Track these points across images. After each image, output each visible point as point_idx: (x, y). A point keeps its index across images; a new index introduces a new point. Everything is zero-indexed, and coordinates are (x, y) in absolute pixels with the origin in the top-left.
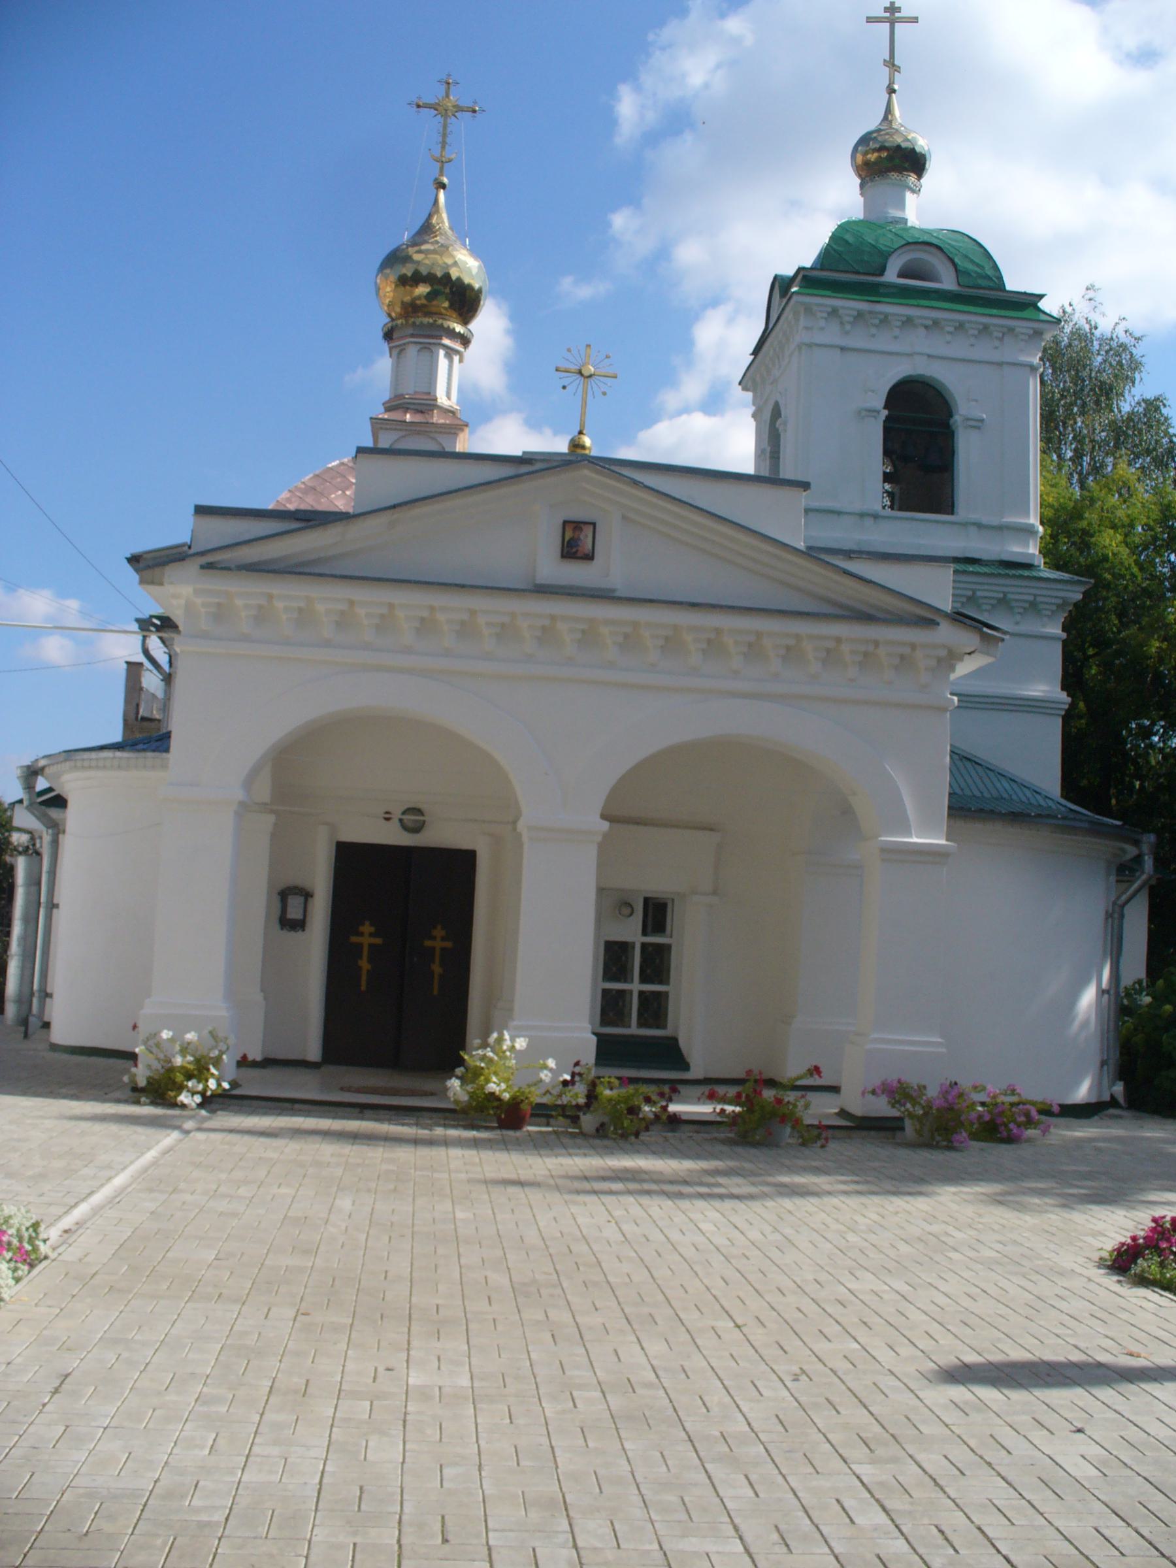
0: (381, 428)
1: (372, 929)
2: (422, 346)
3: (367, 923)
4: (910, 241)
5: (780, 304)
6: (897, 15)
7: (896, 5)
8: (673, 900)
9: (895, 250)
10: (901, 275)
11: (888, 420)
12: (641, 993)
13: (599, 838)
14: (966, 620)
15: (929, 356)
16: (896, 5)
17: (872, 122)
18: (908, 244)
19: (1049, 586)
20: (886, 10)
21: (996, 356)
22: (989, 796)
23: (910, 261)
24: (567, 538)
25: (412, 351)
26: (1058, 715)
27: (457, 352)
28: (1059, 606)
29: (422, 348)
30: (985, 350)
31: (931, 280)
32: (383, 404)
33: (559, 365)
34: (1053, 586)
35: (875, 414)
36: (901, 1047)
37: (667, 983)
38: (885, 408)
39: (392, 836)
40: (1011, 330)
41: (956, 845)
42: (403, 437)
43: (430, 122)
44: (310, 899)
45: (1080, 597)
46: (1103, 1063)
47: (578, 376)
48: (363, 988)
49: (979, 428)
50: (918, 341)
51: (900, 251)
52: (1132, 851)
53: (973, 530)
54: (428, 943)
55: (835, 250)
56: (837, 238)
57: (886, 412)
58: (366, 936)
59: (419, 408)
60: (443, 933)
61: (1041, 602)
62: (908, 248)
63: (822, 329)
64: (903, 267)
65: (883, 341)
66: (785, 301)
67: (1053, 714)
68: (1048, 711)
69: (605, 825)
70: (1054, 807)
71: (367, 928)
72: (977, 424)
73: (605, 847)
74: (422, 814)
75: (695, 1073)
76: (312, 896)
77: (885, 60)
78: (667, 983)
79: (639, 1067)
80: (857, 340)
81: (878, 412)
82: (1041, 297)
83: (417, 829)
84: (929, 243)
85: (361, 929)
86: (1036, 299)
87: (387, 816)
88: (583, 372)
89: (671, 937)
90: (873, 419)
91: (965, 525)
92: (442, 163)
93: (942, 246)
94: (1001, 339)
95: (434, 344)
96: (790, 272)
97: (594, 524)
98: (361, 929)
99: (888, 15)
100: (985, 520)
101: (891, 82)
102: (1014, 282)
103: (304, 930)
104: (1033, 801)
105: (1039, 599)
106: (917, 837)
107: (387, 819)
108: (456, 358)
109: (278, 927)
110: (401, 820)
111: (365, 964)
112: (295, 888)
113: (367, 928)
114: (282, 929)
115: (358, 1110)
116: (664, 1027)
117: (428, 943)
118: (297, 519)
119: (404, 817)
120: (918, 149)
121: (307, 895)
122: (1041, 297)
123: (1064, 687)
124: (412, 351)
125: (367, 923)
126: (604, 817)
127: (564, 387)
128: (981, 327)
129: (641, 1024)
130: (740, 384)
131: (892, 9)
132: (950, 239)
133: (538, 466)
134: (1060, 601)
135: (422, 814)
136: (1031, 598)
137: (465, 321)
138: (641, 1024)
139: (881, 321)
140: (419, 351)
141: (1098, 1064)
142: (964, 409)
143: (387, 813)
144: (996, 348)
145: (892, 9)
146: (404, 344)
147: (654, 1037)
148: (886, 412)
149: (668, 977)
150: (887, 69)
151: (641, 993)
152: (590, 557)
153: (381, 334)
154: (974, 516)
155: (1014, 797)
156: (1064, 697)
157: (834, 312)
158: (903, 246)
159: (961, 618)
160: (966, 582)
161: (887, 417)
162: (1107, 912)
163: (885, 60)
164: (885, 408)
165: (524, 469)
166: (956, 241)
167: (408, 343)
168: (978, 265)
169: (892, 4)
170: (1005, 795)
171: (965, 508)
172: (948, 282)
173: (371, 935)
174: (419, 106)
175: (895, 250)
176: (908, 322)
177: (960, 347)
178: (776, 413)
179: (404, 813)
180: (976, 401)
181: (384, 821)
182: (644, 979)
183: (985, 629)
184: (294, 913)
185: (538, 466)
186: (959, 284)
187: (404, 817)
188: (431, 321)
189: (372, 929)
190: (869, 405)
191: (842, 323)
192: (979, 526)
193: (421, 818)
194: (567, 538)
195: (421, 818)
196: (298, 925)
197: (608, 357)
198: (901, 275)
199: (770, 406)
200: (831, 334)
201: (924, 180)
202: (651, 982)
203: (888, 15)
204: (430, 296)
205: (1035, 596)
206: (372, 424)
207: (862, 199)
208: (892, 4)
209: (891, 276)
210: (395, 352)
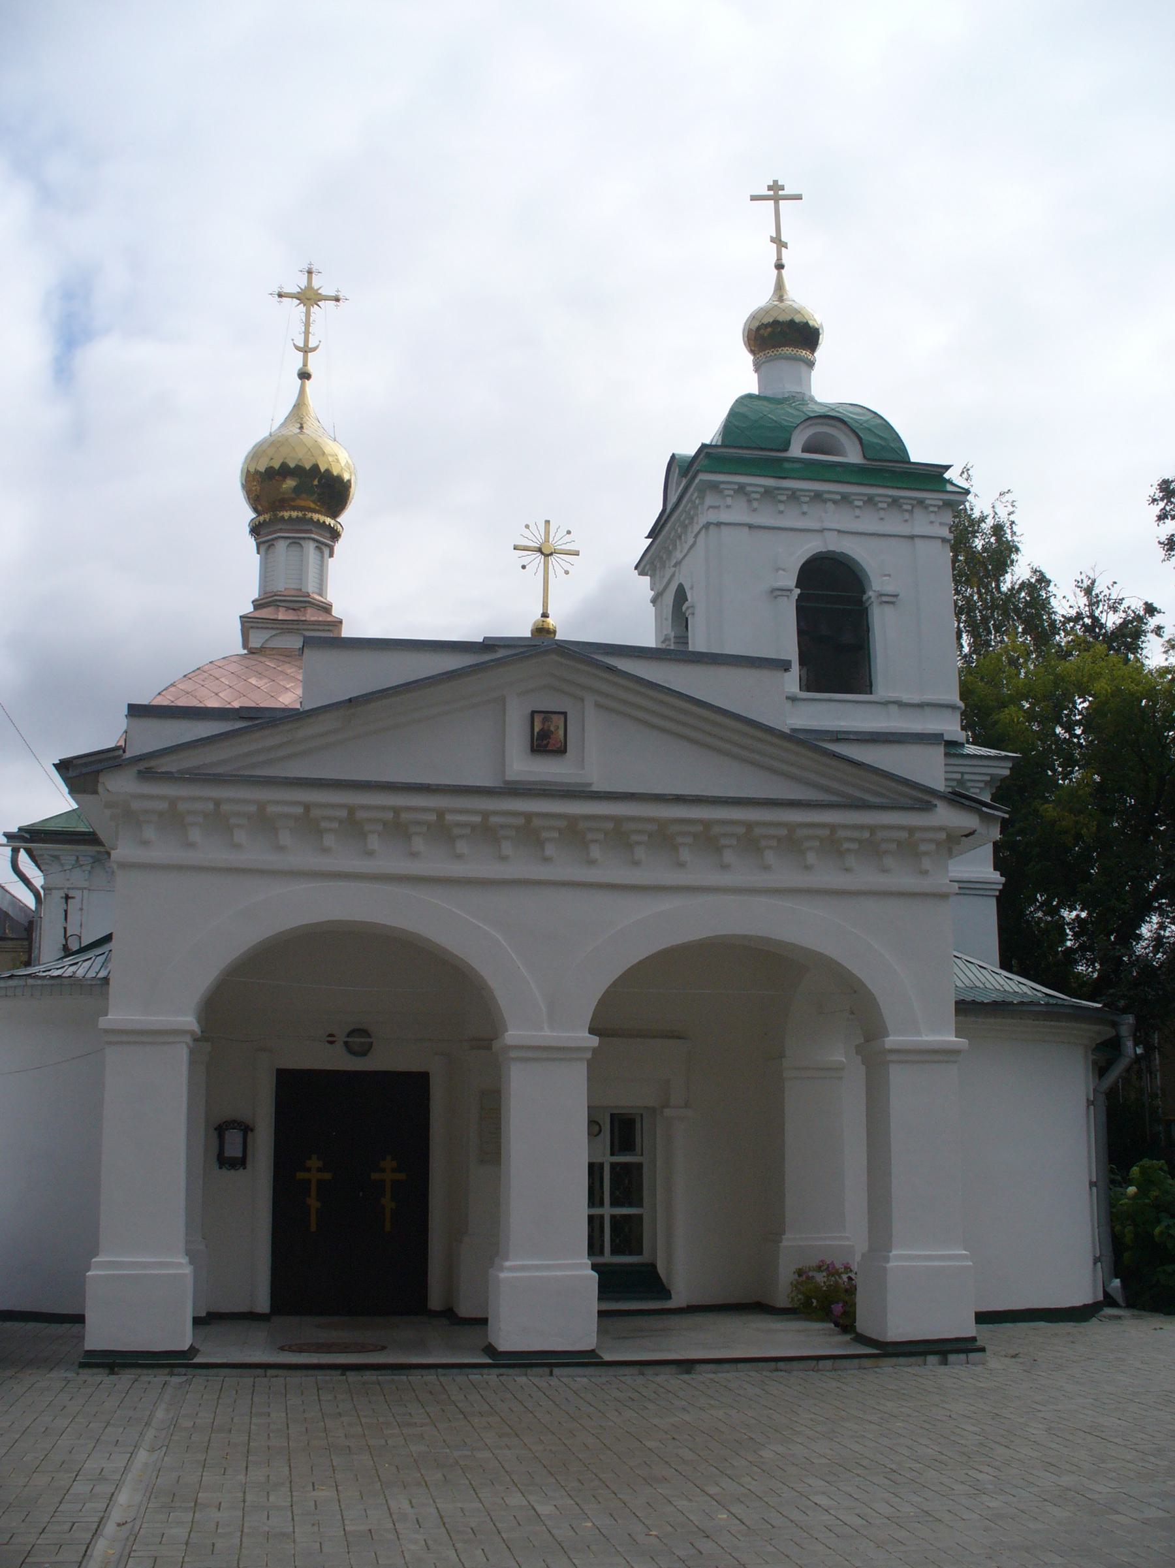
0: (252, 627)
1: (394, 1164)
2: (267, 545)
3: (314, 1157)
4: (812, 415)
5: (678, 485)
6: (781, 193)
7: (780, 183)
8: (642, 1115)
9: (798, 425)
10: (805, 449)
11: (800, 599)
12: (613, 1217)
13: (589, 1055)
14: (963, 801)
15: (839, 531)
16: (780, 183)
17: (759, 298)
18: (810, 418)
19: (981, 764)
20: (770, 188)
21: (905, 530)
22: (962, 985)
23: (810, 437)
24: (536, 730)
25: (281, 546)
26: (994, 896)
27: (326, 545)
28: (986, 783)
29: (290, 543)
30: (893, 523)
31: (834, 455)
32: (253, 602)
33: (517, 544)
34: (986, 763)
35: (788, 593)
36: (936, 1263)
37: (640, 1204)
38: (797, 587)
39: (337, 1060)
40: (921, 502)
41: (967, 1041)
42: (274, 635)
43: (296, 310)
44: (250, 1134)
45: (1007, 772)
46: (1096, 1260)
47: (539, 554)
48: (313, 1228)
49: (893, 603)
50: (835, 518)
51: (801, 427)
52: (1109, 1032)
53: (894, 709)
54: (301, 1175)
55: (737, 427)
56: (733, 414)
57: (798, 591)
58: (314, 1171)
59: (296, 605)
60: (320, 1164)
61: (969, 780)
62: (809, 422)
63: (728, 507)
64: (803, 445)
65: (791, 519)
66: (684, 482)
67: (986, 895)
68: (982, 892)
69: (594, 1041)
70: (1029, 993)
71: (314, 1163)
72: (890, 600)
73: (596, 1065)
74: (370, 1036)
75: (678, 1300)
76: (252, 1130)
77: (771, 237)
78: (640, 1204)
79: (617, 1300)
80: (765, 517)
81: (791, 591)
82: (947, 467)
83: (364, 1051)
84: (833, 418)
85: (309, 1163)
86: (944, 470)
87: (330, 1039)
88: (543, 550)
89: (642, 1155)
90: (786, 598)
91: (886, 703)
92: (306, 350)
93: (845, 419)
94: (911, 512)
95: (304, 538)
96: (690, 450)
97: (565, 714)
98: (309, 1163)
99: (771, 193)
100: (906, 697)
101: (779, 258)
102: (919, 453)
103: (245, 1168)
104: (1007, 988)
105: (967, 777)
106: (927, 1036)
107: (331, 1043)
108: (326, 551)
109: (216, 1166)
110: (346, 1043)
111: (314, 1203)
112: (234, 1121)
113: (314, 1163)
114: (220, 1168)
115: (339, 1372)
116: (640, 1253)
117: (301, 1175)
118: (242, 718)
119: (350, 1040)
120: (811, 323)
121: (246, 1129)
122: (947, 467)
123: (996, 867)
124: (281, 546)
125: (314, 1157)
126: (592, 1031)
127: (524, 567)
128: (890, 500)
129: (614, 1252)
130: (636, 568)
131: (775, 187)
132: (851, 413)
133: (501, 653)
134: (988, 778)
135: (370, 1036)
136: (958, 776)
137: (335, 515)
138: (614, 1252)
139: (789, 497)
140: (288, 546)
141: (1091, 1263)
142: (877, 584)
143: (331, 1035)
144: (906, 521)
145: (775, 187)
146: (273, 540)
147: (631, 1265)
148: (798, 591)
149: (641, 1199)
150: (775, 245)
151: (613, 1217)
152: (562, 751)
153: (248, 529)
154: (893, 695)
155: (988, 985)
156: (996, 877)
157: (741, 489)
158: (805, 420)
159: (958, 799)
160: (286, 803)
161: (799, 596)
162: (1088, 1100)
163: (771, 237)
164: (797, 587)
165: (486, 657)
166: (854, 414)
167: (276, 538)
168: (881, 438)
169: (776, 182)
170: (978, 984)
171: (883, 689)
172: (853, 456)
173: (319, 1170)
174: (280, 295)
175: (798, 425)
176: (818, 497)
177: (868, 522)
178: (681, 596)
179: (348, 1036)
180: (889, 575)
181: (328, 1045)
182: (615, 1203)
183: (984, 809)
184: (233, 1150)
185: (501, 653)
186: (865, 457)
187: (350, 1040)
188: (300, 514)
189: (394, 1164)
190: (779, 584)
191: (749, 501)
192: (900, 704)
193: (369, 1040)
194: (536, 730)
195: (369, 1040)
196: (240, 1163)
197: (569, 532)
198: (805, 449)
199: (673, 587)
200: (737, 512)
201: (818, 354)
202: (622, 1205)
203: (771, 193)
204: (297, 490)
205: (962, 774)
206: (243, 623)
207: (755, 376)
208: (776, 182)
209: (795, 451)
210: (263, 548)
